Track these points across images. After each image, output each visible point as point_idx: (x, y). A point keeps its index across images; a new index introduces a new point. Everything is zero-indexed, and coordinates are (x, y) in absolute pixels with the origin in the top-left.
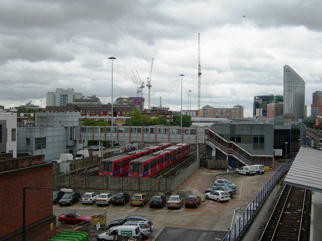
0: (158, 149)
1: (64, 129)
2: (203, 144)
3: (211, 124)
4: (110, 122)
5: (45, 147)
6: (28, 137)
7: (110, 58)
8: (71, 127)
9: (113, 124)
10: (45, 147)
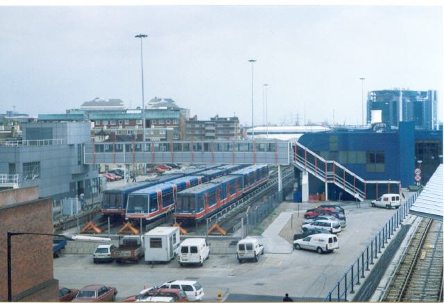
0: (221, 174)
2: (288, 167)
3: (299, 136)
4: (140, 137)
6: (12, 161)
9: (146, 140)
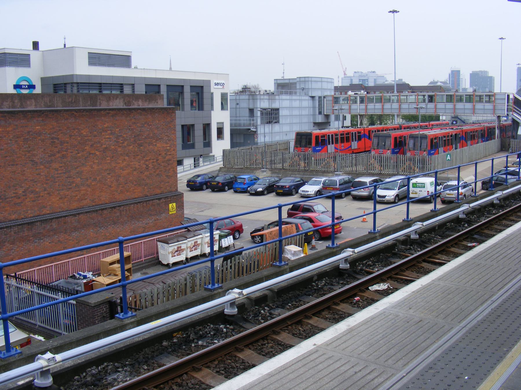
1: (310, 98)
5: (278, 122)
6: (251, 107)
7: (390, 12)
8: (320, 97)
10: (278, 122)
